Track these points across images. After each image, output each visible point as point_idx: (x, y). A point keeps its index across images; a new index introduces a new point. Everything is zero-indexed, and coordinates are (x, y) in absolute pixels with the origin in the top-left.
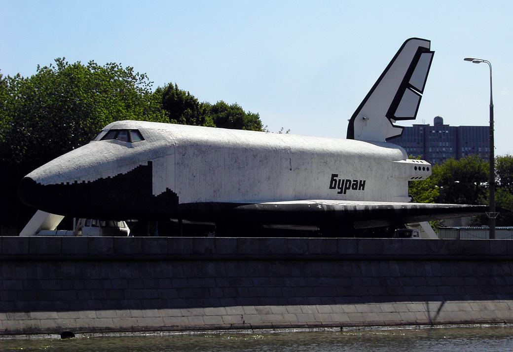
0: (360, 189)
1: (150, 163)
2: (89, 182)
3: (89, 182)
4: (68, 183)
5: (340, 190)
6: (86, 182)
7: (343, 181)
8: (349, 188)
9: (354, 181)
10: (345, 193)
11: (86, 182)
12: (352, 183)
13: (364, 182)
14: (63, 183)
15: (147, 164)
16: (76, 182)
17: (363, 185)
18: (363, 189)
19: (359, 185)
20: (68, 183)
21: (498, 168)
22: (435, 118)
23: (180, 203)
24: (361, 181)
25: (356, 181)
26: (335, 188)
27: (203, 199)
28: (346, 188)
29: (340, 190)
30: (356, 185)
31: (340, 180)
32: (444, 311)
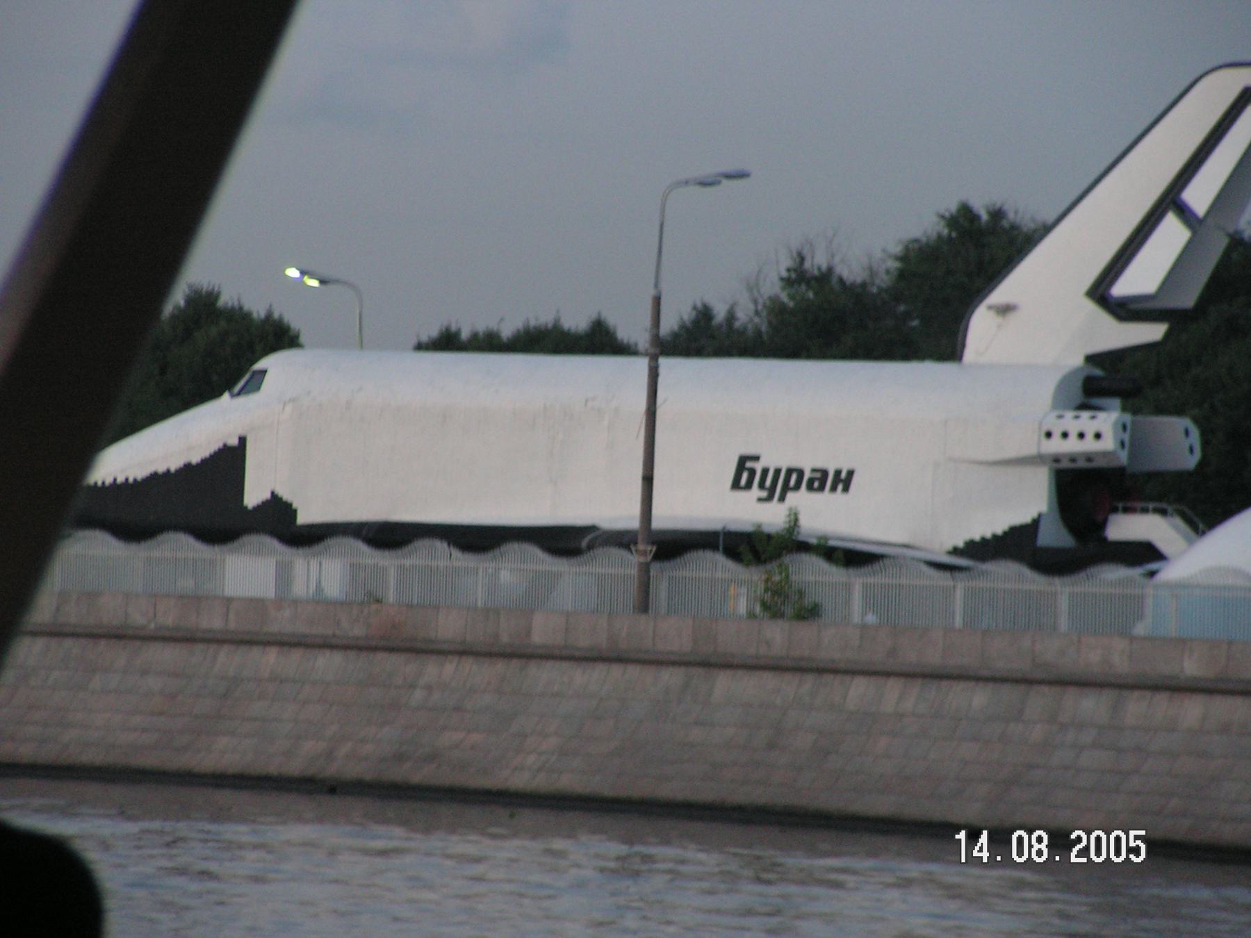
5: (749, 464)
8: (797, 486)
9: (814, 470)
13: (851, 473)
24: (838, 473)
25: (825, 473)
26: (749, 486)
28: (786, 488)
29: (749, 464)
31: (765, 472)
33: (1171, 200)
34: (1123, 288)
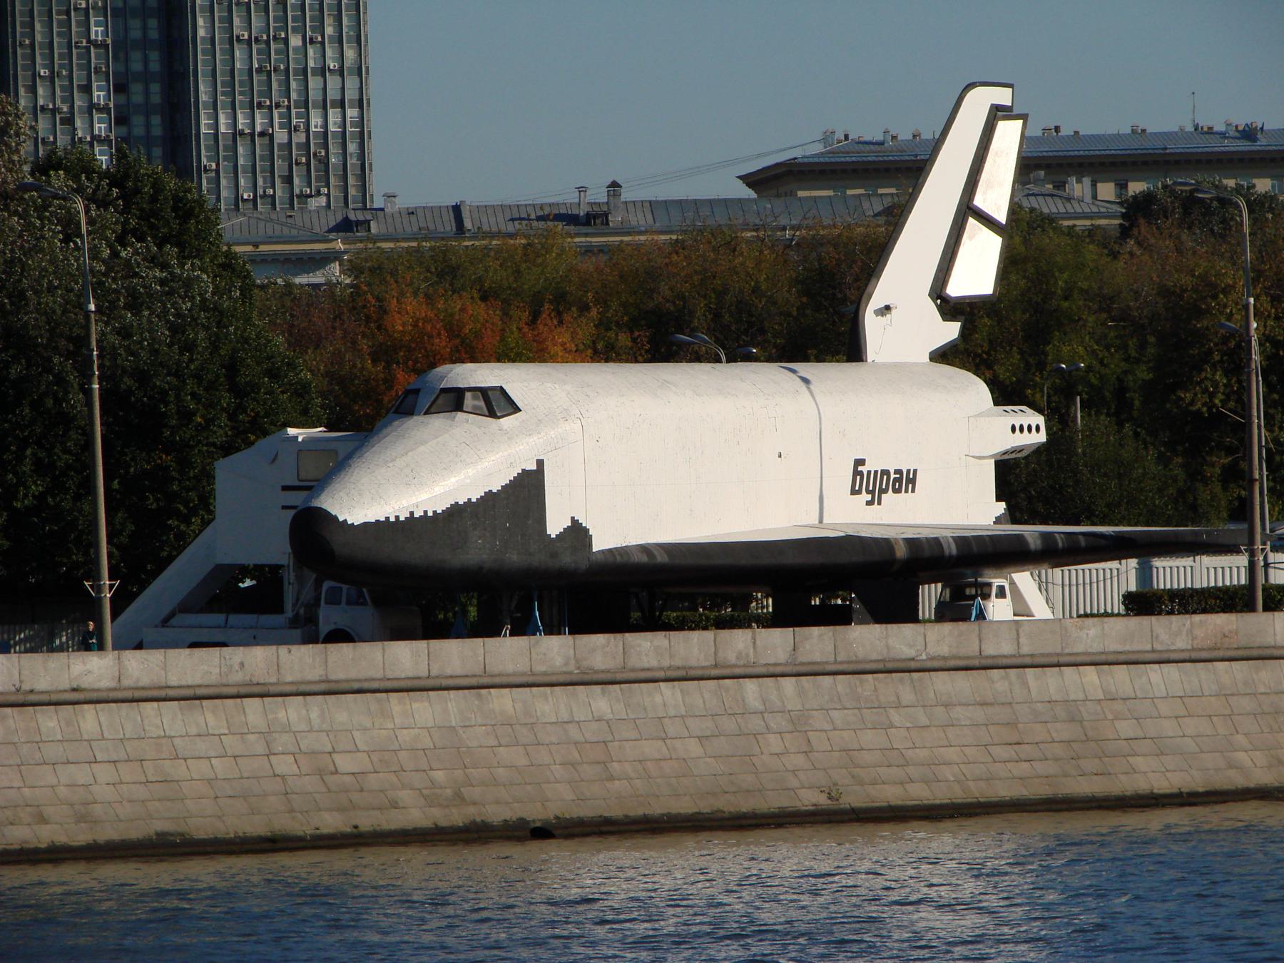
0: (906, 491)
1: (540, 463)
2: (435, 512)
3: (435, 512)
4: (397, 517)
6: (430, 514)
7: (876, 472)
8: (886, 491)
9: (897, 472)
10: (879, 503)
11: (430, 514)
12: (893, 476)
13: (915, 471)
14: (388, 518)
15: (535, 468)
16: (412, 513)
17: (912, 481)
18: (913, 491)
19: (904, 481)
20: (397, 517)
21: (330, 428)
22: (944, 320)
23: (553, 536)
24: (908, 471)
26: (859, 492)
27: (895, 626)
29: (869, 497)
30: (899, 480)
31: (869, 472)
32: (754, 638)
33: (967, 210)
34: (957, 288)
